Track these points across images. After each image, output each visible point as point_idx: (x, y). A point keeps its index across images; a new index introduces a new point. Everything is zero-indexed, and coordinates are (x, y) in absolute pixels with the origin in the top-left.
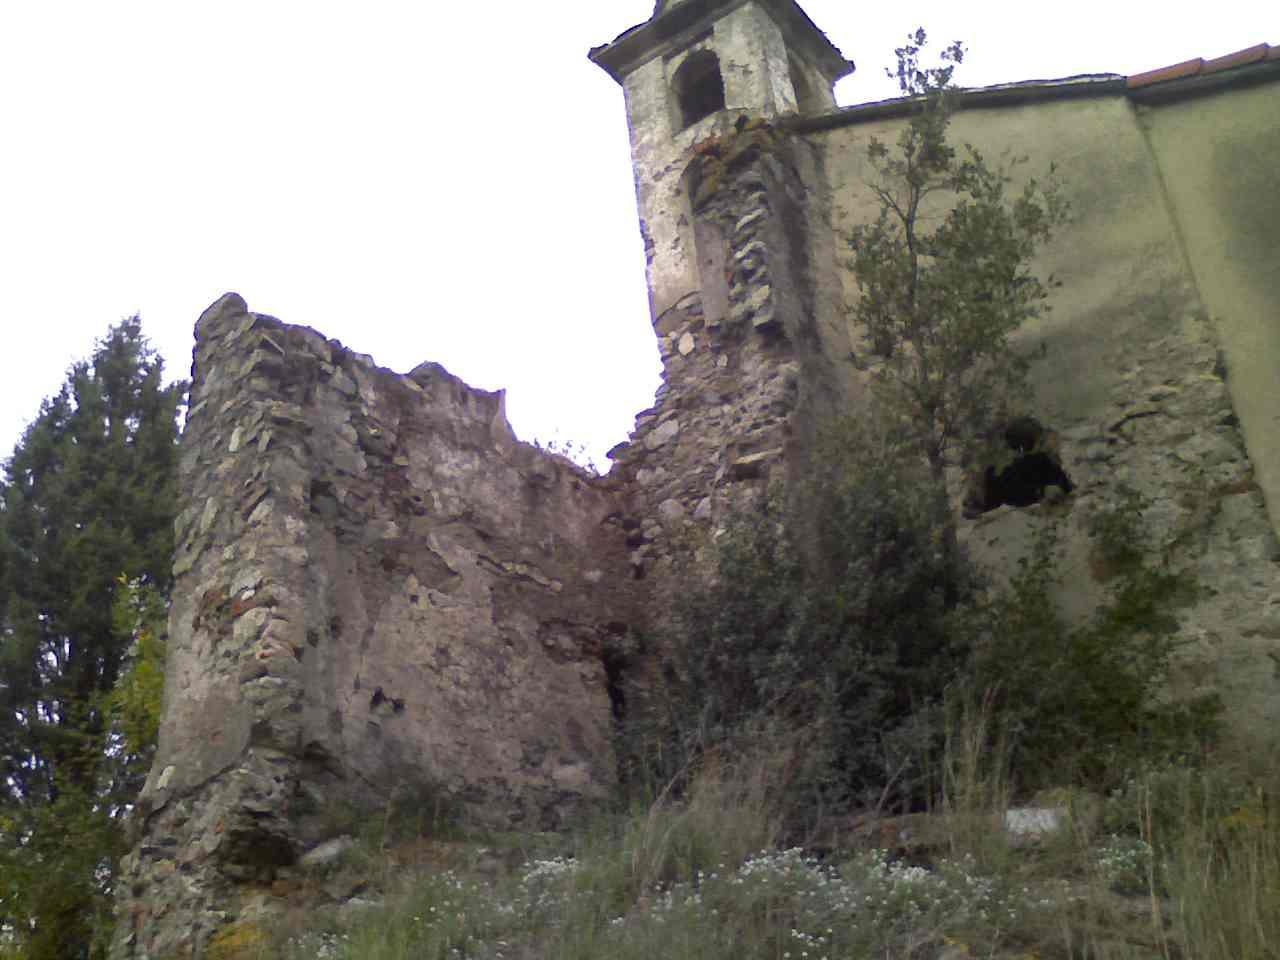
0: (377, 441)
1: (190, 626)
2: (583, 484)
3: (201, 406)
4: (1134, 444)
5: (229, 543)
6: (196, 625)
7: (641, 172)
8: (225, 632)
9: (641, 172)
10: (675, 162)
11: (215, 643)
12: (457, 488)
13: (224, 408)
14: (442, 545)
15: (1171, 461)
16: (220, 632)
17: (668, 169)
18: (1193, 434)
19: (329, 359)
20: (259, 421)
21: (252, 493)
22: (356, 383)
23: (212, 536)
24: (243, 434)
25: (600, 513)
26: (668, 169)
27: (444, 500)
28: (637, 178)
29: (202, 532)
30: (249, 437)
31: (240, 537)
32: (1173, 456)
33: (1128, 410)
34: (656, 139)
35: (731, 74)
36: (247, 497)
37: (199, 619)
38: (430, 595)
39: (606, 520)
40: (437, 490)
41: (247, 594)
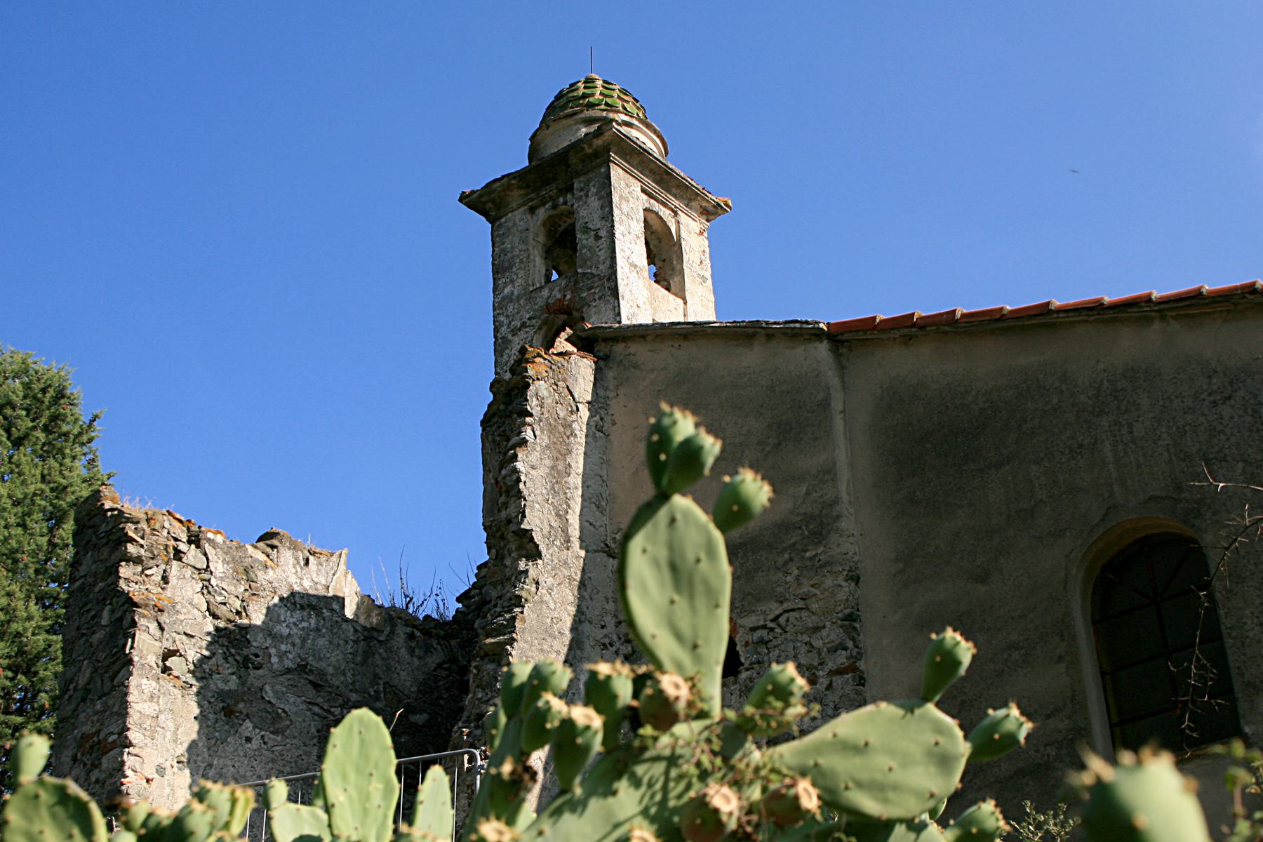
0: (223, 606)
1: (68, 759)
2: (418, 633)
3: (78, 583)
4: (785, 632)
5: (100, 698)
6: (75, 759)
7: (501, 324)
8: (95, 765)
9: (501, 324)
10: (529, 319)
11: (89, 772)
12: (293, 645)
13: (97, 589)
14: (275, 692)
15: (807, 648)
16: (92, 764)
17: (523, 325)
18: (824, 627)
19: (185, 540)
20: (123, 604)
21: (117, 660)
22: (208, 559)
23: (88, 691)
24: (113, 612)
25: (433, 660)
26: (523, 325)
27: (282, 655)
28: (496, 330)
29: (80, 687)
30: (118, 614)
31: (108, 693)
32: (809, 644)
33: (786, 606)
34: (516, 293)
35: (585, 236)
36: (114, 663)
37: (76, 754)
38: (262, 737)
39: (439, 666)
40: (275, 647)
41: (111, 738)
